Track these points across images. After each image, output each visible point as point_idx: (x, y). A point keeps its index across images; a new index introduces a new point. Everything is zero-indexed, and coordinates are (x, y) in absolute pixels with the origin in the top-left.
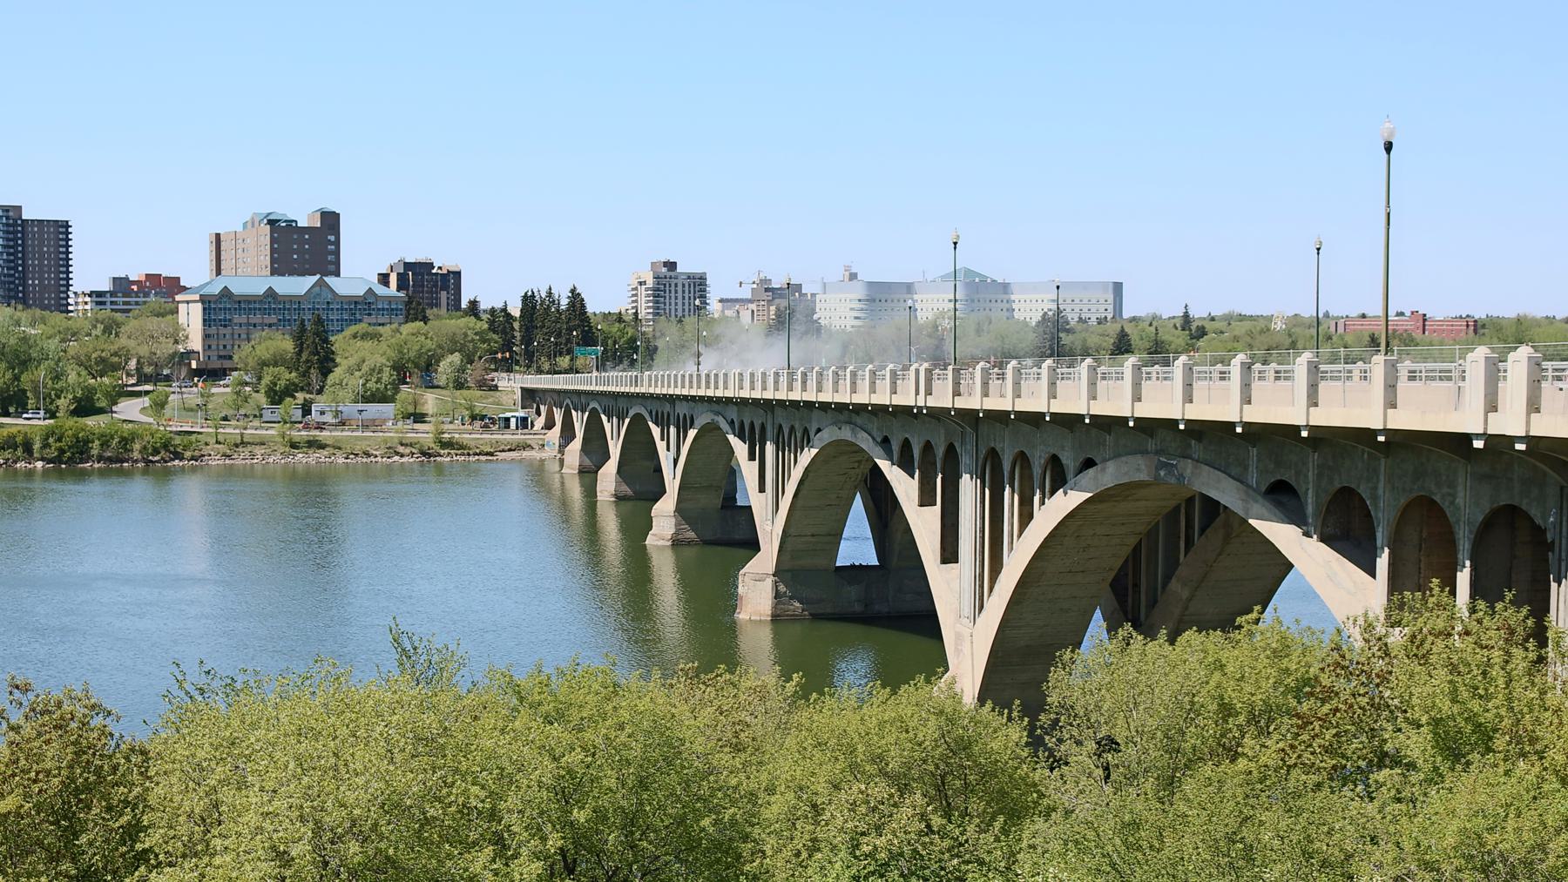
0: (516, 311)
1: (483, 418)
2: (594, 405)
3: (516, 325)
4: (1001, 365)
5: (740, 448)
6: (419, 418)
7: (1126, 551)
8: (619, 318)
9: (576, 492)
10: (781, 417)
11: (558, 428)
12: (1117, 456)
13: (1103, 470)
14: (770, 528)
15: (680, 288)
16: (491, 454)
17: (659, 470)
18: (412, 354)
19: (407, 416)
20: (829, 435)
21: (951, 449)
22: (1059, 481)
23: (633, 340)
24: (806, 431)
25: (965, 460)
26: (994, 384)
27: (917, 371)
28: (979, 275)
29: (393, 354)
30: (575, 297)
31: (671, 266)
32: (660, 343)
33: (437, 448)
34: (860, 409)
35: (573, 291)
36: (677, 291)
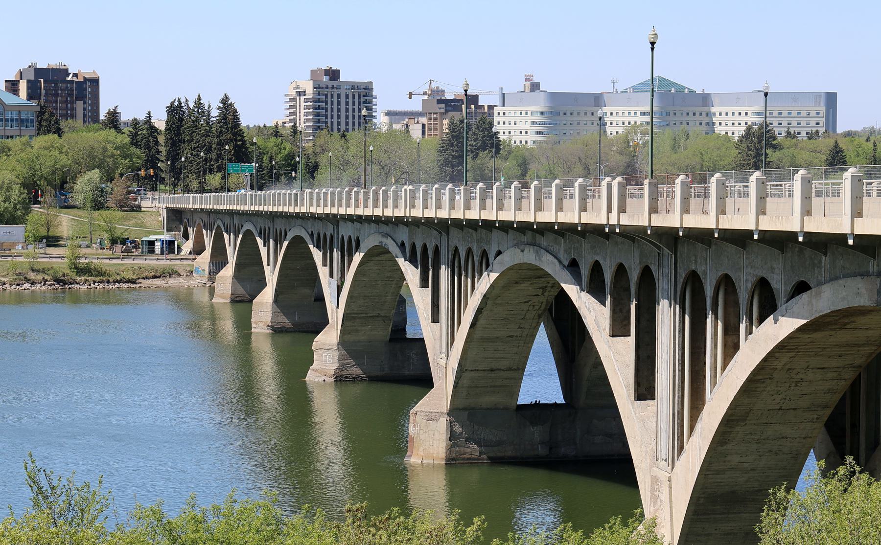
0: (160, 122)
1: (124, 241)
2: (248, 226)
3: (161, 139)
4: (704, 180)
5: (411, 274)
6: (53, 241)
7: (843, 385)
8: (276, 132)
9: (228, 326)
10: (457, 239)
11: (207, 254)
12: (834, 279)
13: (819, 294)
14: (444, 363)
15: (343, 100)
16: (133, 281)
17: (321, 299)
18: (45, 171)
19: (39, 239)
20: (512, 257)
21: (647, 275)
22: (768, 306)
23: (291, 156)
24: (484, 254)
25: (663, 284)
26: (694, 202)
27: (609, 186)
28: (675, 85)
29: (22, 170)
30: (227, 107)
31: (333, 74)
32: (323, 161)
33: (73, 275)
34: (545, 229)
35: (225, 100)
36: (339, 102)
